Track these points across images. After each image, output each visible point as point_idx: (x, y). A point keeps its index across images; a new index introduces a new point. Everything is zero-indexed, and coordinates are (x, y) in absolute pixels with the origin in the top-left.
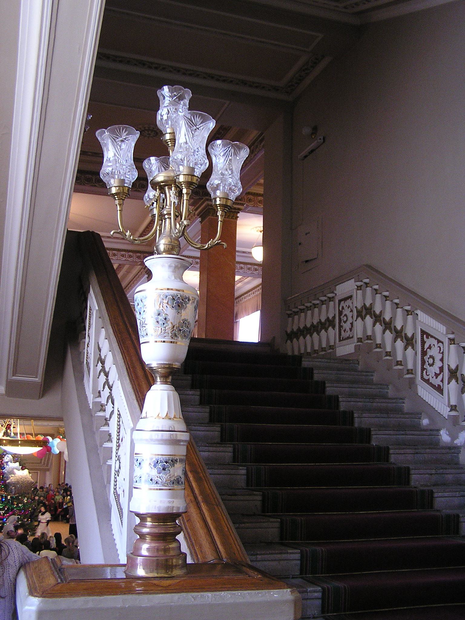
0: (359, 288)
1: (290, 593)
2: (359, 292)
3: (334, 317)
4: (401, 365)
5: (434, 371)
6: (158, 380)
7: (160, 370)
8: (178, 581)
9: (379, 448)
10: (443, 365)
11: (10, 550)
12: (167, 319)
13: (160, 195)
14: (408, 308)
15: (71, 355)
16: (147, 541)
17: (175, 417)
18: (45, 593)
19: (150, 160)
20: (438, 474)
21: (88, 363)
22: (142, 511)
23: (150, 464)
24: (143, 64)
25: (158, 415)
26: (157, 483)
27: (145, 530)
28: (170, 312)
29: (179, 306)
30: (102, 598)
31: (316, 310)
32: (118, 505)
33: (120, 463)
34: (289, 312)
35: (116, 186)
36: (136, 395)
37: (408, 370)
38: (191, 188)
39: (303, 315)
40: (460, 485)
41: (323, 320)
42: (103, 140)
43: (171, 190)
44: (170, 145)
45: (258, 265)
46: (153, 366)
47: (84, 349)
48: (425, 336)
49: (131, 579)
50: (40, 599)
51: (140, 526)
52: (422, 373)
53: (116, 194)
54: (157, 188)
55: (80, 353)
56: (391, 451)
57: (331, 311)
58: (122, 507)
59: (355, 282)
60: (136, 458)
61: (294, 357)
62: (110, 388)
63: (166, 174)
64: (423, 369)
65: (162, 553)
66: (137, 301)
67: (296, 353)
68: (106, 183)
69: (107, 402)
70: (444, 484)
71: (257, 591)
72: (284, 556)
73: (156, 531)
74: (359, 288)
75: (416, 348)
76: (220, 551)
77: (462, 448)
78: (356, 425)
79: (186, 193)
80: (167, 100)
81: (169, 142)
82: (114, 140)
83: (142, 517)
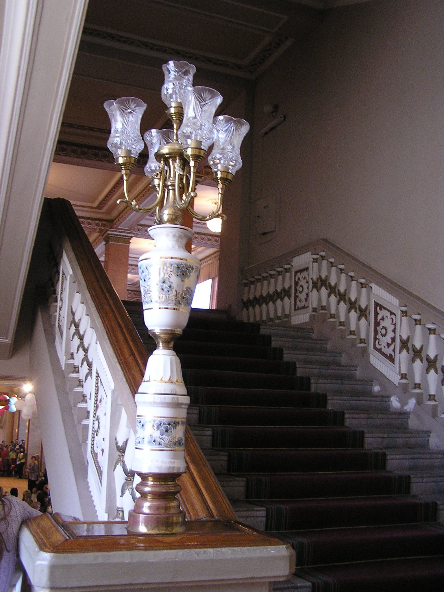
0: (315, 260)
1: (286, 549)
2: (316, 264)
3: (290, 288)
4: (354, 334)
5: (386, 341)
6: (161, 345)
7: (162, 335)
8: (179, 538)
9: (335, 413)
10: (395, 335)
11: (12, 506)
12: (172, 287)
13: (164, 167)
14: (362, 281)
15: (42, 318)
16: (148, 499)
17: (177, 381)
18: (56, 549)
19: (151, 132)
20: (389, 437)
21: (60, 326)
22: (145, 471)
23: (153, 426)
24: (112, 37)
25: (162, 379)
26: (160, 444)
27: (147, 489)
28: (174, 280)
29: (183, 274)
30: (110, 553)
31: (273, 280)
32: (96, 463)
33: (99, 423)
34: (245, 281)
35: (123, 156)
36: (117, 358)
37: (361, 340)
38: (198, 161)
39: (259, 284)
40: (409, 448)
41: (279, 290)
42: (112, 111)
43: (176, 162)
44: (175, 119)
45: (214, 235)
46: (156, 331)
47: (56, 311)
48: (378, 308)
49: (133, 535)
50: (52, 554)
51: (142, 485)
53: (123, 164)
54: (162, 159)
55: (51, 316)
56: (346, 416)
57: (288, 282)
58: (100, 466)
59: (312, 254)
60: (139, 420)
61: (253, 325)
62: (86, 351)
63: (171, 147)
64: (375, 339)
65: (163, 511)
66: (142, 269)
67: (252, 320)
68: (113, 152)
69: (82, 364)
70: (395, 447)
71: (255, 548)
72: (250, 513)
73: (157, 489)
74: (315, 260)
75: (369, 319)
76: (211, 509)
77: (412, 414)
78: (313, 390)
79: (193, 167)
80: (173, 74)
81: (173, 115)
82: (123, 112)
83: (144, 477)
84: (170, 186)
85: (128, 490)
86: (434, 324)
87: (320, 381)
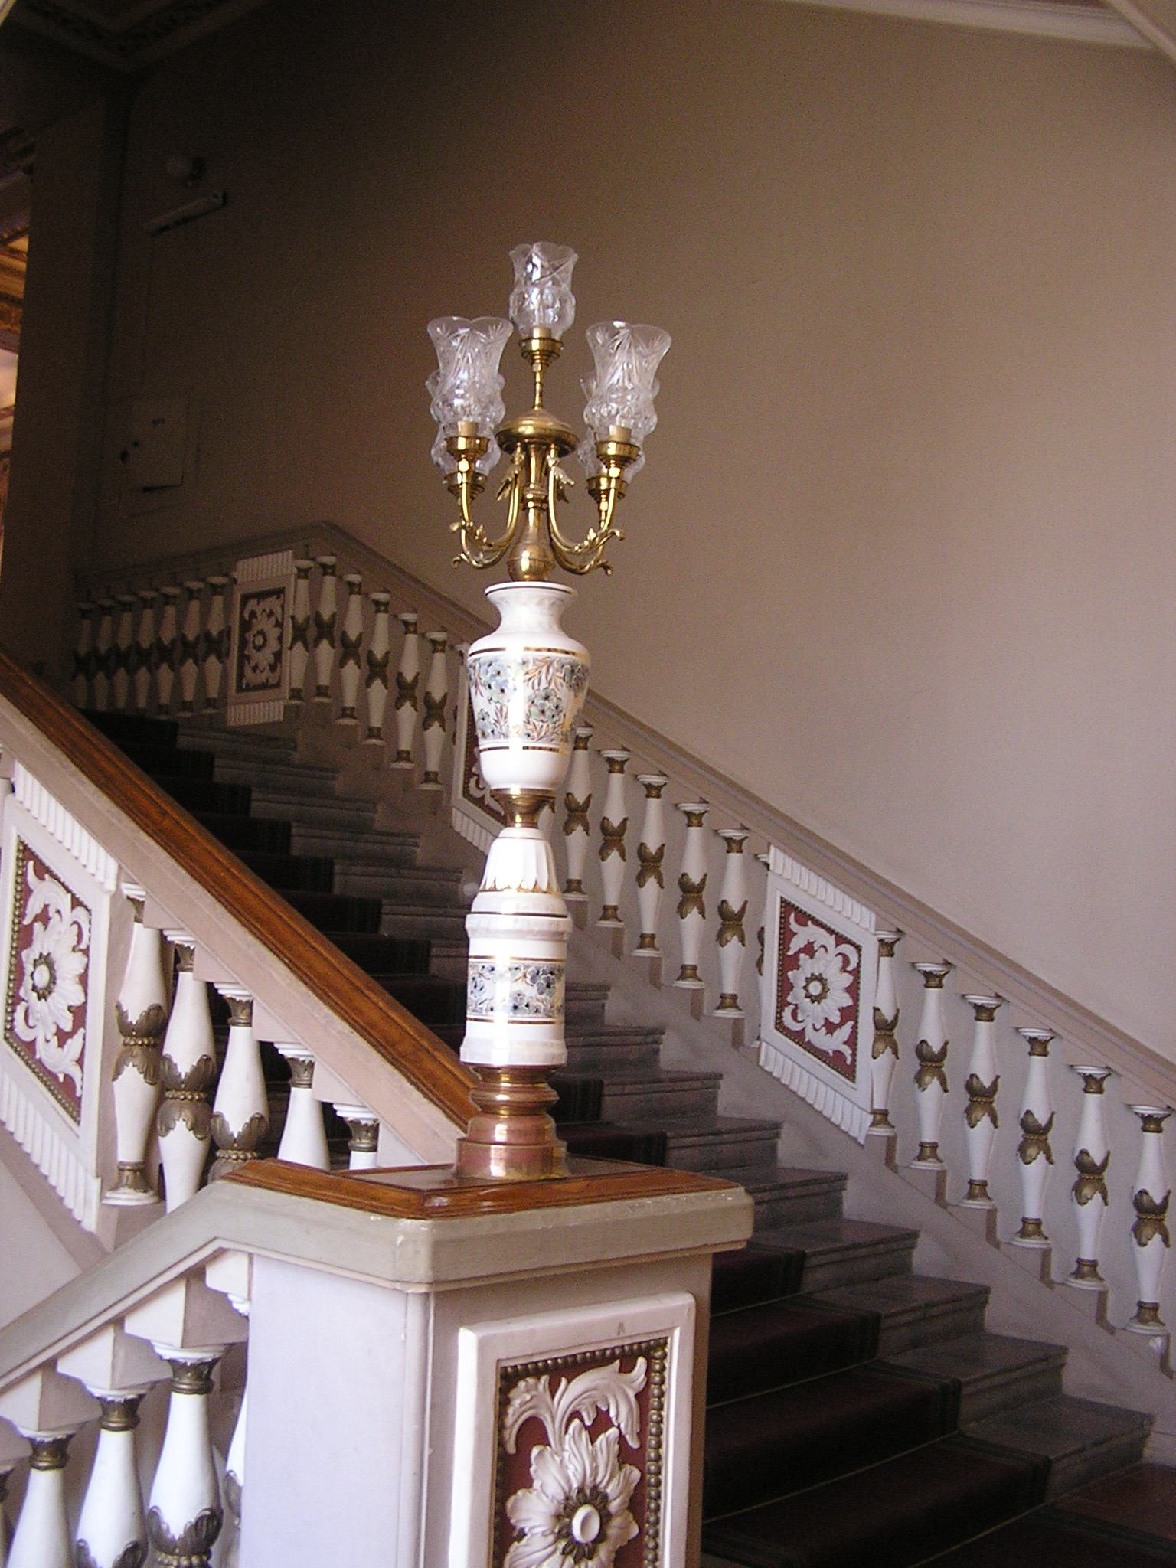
2: (303, 584)
6: (518, 818)
12: (560, 709)
14: (438, 636)
17: (536, 889)
26: (537, 1011)
28: (563, 692)
30: (512, 1215)
34: (82, 605)
52: (466, 782)
59: (296, 557)
74: (303, 573)
78: (337, 891)
84: (532, 500)
85: (181, 1119)
86: (625, 749)
87: (354, 869)
